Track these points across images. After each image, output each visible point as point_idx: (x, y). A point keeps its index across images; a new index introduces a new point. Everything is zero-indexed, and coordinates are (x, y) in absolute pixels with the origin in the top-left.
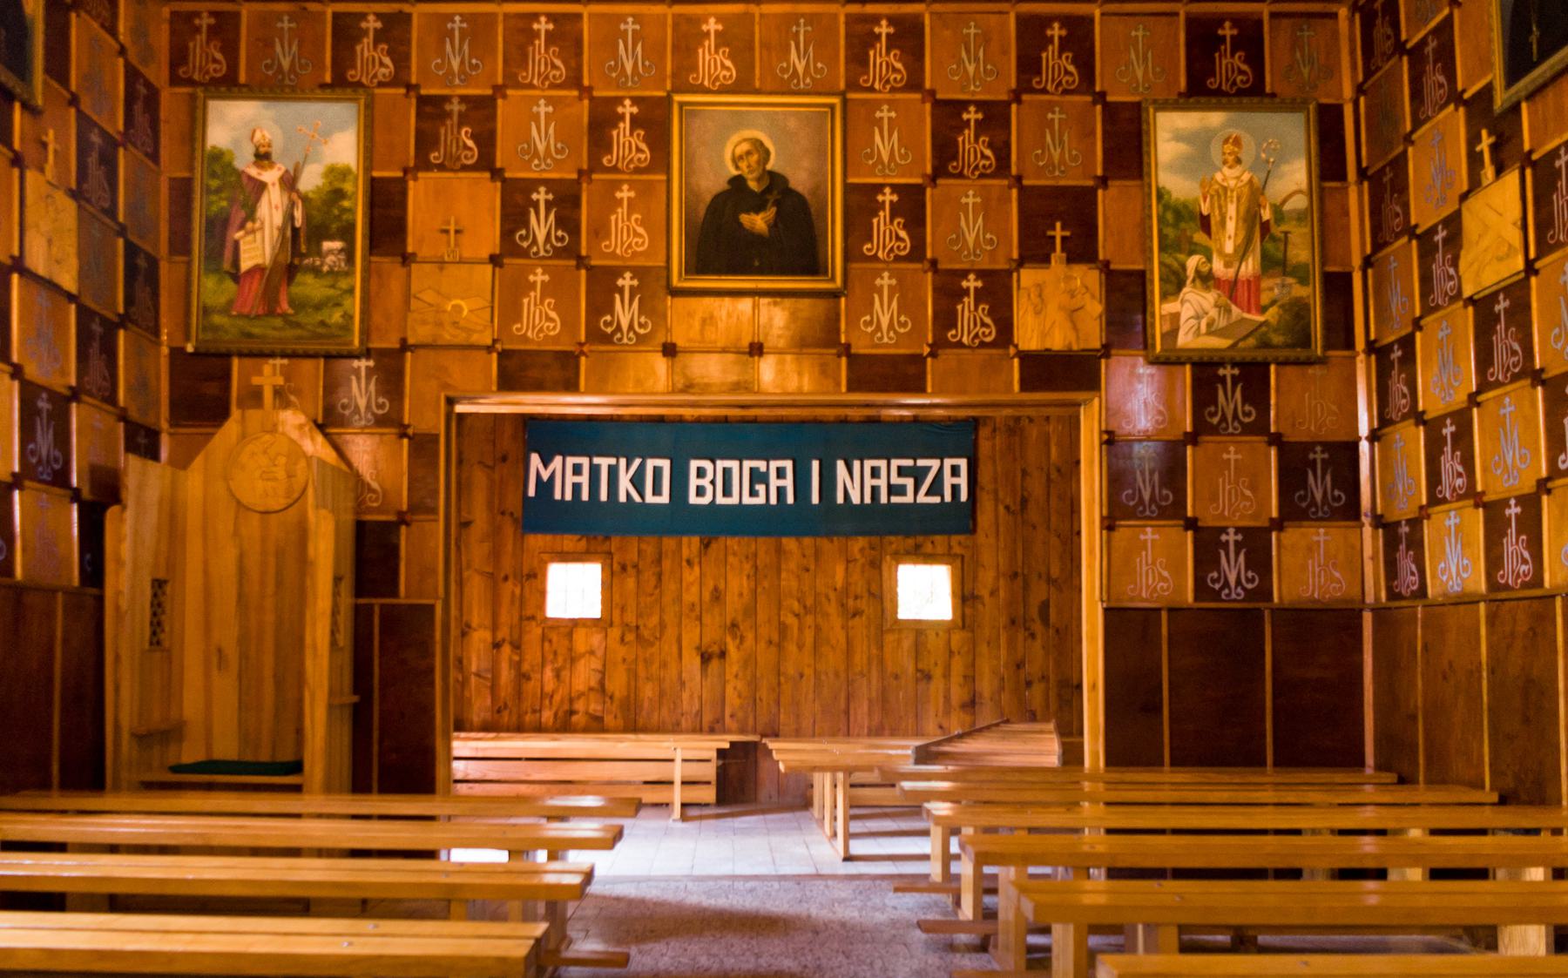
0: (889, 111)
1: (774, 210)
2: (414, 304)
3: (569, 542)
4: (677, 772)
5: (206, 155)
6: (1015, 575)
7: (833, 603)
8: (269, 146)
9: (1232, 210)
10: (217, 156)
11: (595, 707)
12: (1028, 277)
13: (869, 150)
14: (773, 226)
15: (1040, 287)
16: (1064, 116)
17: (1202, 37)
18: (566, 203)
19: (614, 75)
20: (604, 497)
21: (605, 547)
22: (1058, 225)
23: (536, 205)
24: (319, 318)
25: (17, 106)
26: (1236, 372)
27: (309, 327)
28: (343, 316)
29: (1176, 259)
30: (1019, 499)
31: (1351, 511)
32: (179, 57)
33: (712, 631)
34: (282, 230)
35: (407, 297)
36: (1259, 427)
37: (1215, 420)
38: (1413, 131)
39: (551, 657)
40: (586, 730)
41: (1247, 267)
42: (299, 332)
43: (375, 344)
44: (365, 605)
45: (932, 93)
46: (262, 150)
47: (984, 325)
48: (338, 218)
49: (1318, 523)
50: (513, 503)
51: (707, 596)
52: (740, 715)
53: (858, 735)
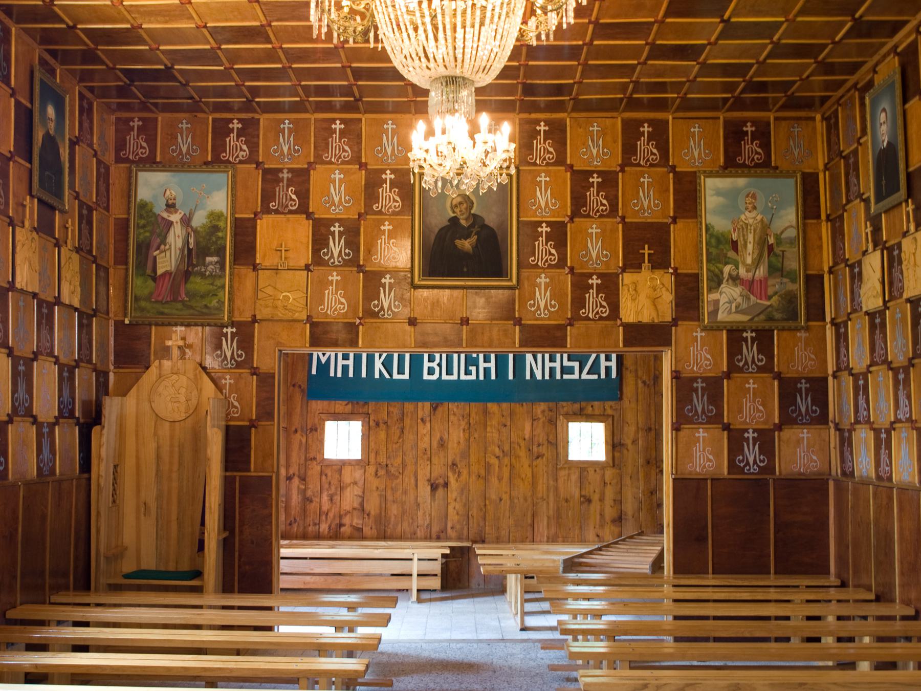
0: (545, 177)
1: (476, 237)
2: (260, 295)
3: (340, 406)
4: (415, 568)
5: (137, 203)
6: (650, 429)
7: (523, 447)
8: (174, 199)
9: (750, 238)
10: (143, 205)
11: (357, 522)
12: (628, 278)
13: (533, 200)
14: (475, 247)
15: (635, 284)
16: (651, 180)
17: (734, 135)
18: (352, 234)
19: (380, 155)
20: (364, 375)
21: (365, 410)
22: (646, 246)
23: (333, 233)
24: (204, 303)
25: (57, 212)
26: (754, 334)
27: (198, 309)
28: (217, 302)
29: (717, 267)
30: (652, 377)
31: (823, 419)
32: (121, 145)
33: (438, 470)
34: (182, 250)
35: (256, 290)
36: (767, 368)
37: (741, 364)
38: (846, 204)
39: (327, 486)
40: (351, 538)
41: (759, 271)
42: (192, 311)
43: (237, 318)
44: (230, 476)
45: (571, 166)
46: (170, 202)
47: (602, 306)
48: (215, 243)
49: (803, 427)
50: (301, 378)
51: (435, 444)
52: (458, 527)
53: (541, 541)
